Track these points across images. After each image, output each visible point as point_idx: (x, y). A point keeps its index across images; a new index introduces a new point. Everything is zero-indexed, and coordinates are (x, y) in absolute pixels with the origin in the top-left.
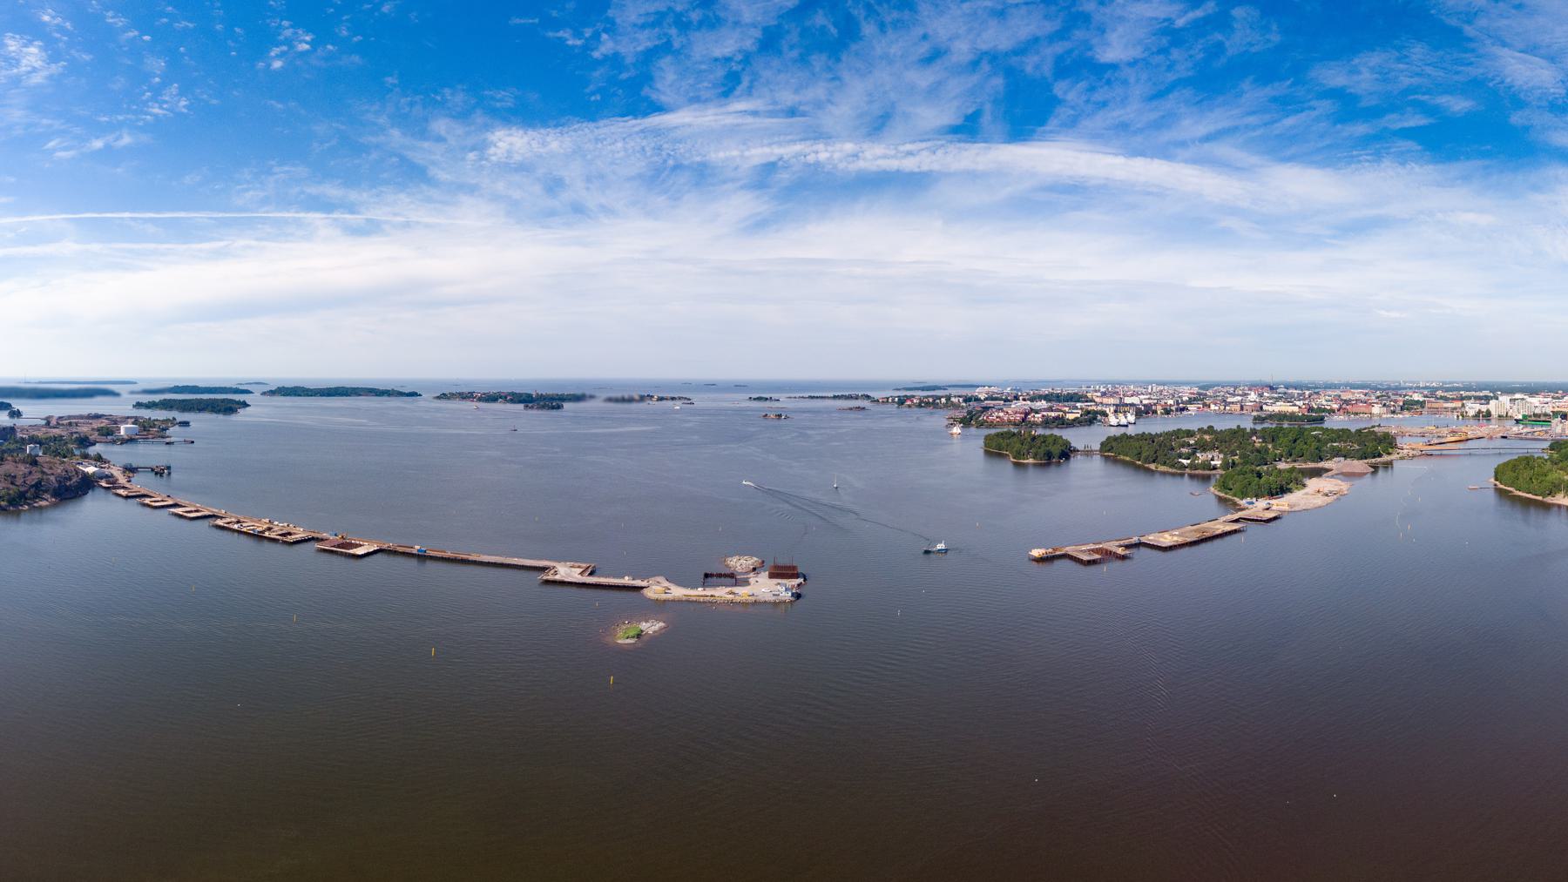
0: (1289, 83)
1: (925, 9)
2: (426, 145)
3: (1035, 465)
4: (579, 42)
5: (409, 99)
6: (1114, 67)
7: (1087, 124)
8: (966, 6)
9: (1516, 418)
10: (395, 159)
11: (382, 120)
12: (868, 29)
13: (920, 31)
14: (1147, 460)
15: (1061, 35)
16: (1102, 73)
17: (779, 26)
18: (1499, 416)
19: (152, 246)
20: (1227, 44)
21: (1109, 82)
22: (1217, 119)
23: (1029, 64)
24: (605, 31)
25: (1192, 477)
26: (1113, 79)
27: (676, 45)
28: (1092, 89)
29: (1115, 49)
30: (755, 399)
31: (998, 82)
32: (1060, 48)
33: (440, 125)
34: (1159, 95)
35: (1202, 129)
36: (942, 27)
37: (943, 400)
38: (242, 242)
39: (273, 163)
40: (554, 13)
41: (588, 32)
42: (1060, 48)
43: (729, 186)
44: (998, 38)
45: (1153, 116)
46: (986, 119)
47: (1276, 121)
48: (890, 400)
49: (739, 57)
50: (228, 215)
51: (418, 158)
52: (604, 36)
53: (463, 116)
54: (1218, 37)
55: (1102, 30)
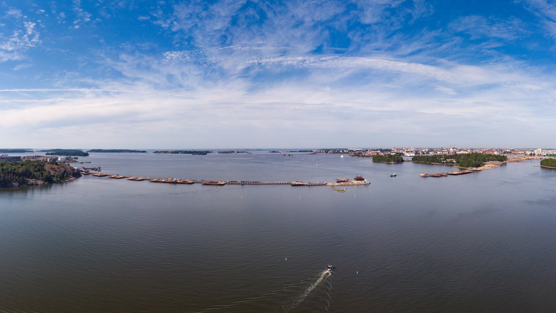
0: (441, 30)
1: (289, 4)
2: (120, 64)
3: (394, 163)
4: (167, 26)
5: (110, 47)
6: (369, 25)
7: (363, 49)
8: (306, 3)
9: (544, 155)
10: (110, 69)
11: (102, 55)
12: (270, 15)
13: (290, 14)
14: (431, 162)
15: (346, 13)
16: (365, 28)
17: (237, 15)
18: (538, 155)
19: (27, 101)
20: (413, 14)
21: (368, 32)
22: (415, 46)
23: (337, 25)
24: (175, 20)
25: (447, 165)
26: (370, 30)
27: (199, 25)
28: (362, 35)
29: (368, 18)
30: (272, 152)
31: (326, 33)
32: (346, 18)
33: (123, 56)
34: (389, 36)
35: (410, 50)
36: (300, 11)
37: (341, 151)
38: (59, 99)
39: (66, 71)
40: (155, 15)
41: (169, 21)
42: (346, 18)
43: (234, 77)
44: (322, 15)
45: (389, 45)
46: (325, 48)
47: (439, 47)
48: (322, 152)
49: (224, 29)
50: (60, 90)
51: (118, 69)
52: (175, 23)
53: (132, 53)
54: (409, 11)
55: (362, 10)
